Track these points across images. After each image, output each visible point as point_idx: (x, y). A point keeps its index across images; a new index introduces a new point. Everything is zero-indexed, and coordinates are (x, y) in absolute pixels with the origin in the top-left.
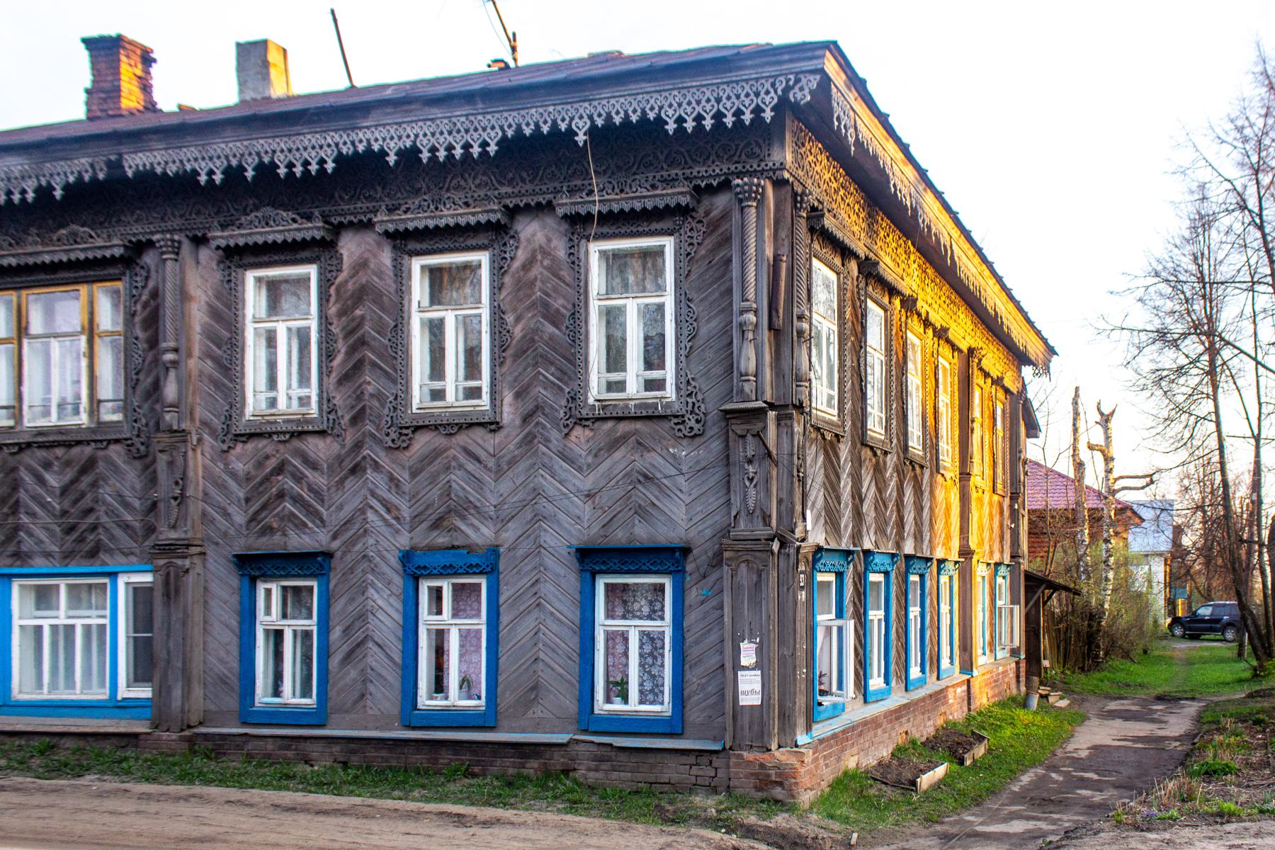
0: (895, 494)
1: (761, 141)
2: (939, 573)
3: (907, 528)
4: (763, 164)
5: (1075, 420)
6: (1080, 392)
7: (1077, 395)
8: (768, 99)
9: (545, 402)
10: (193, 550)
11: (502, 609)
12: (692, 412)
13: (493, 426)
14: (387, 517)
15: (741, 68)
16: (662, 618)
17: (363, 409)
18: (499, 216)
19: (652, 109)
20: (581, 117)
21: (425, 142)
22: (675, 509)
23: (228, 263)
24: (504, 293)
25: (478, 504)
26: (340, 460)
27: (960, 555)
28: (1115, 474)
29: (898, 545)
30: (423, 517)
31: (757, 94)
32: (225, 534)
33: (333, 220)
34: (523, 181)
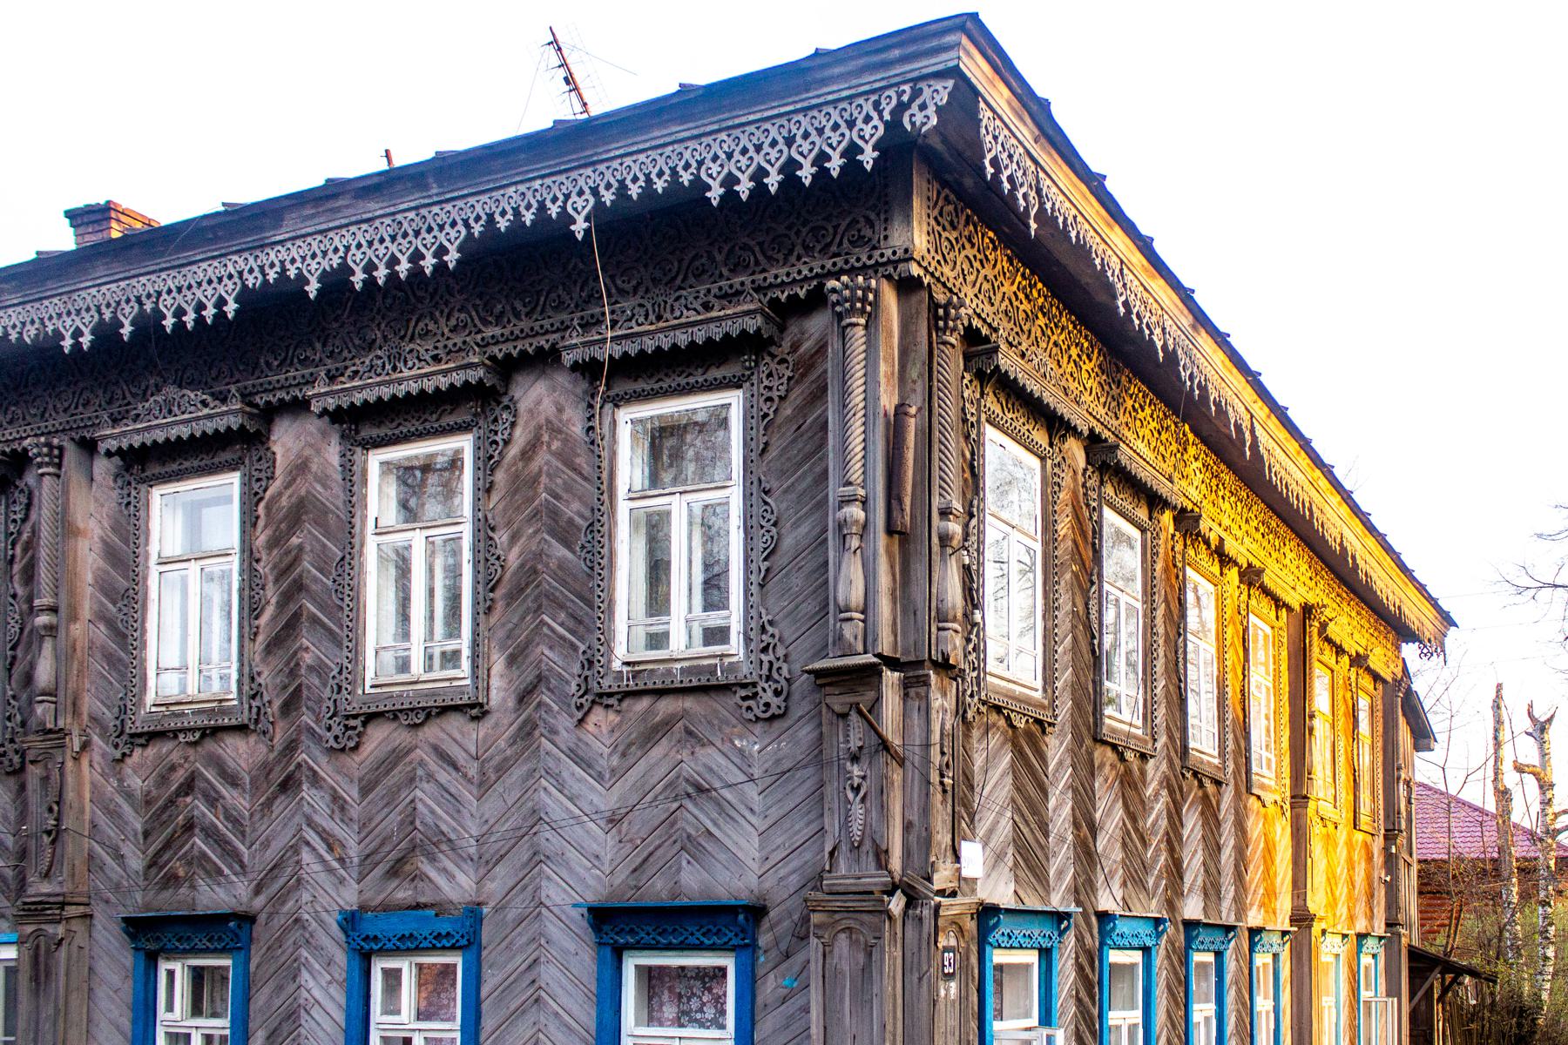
0: (1164, 823)
1: (873, 216)
2: (1251, 950)
3: (1188, 879)
4: (876, 253)
5: (1496, 730)
6: (1504, 693)
7: (1499, 695)
8: (868, 130)
9: (551, 670)
10: (71, 911)
11: (485, 1006)
12: (769, 678)
13: (476, 710)
14: (328, 857)
15: (824, 82)
16: (723, 1027)
17: (298, 689)
18: (481, 372)
19: (687, 166)
20: (581, 193)
21: (359, 256)
22: (742, 842)
23: (127, 477)
24: (495, 497)
25: (453, 837)
26: (266, 769)
27: (1292, 921)
28: (1556, 808)
29: (1171, 906)
30: (378, 857)
31: (851, 124)
32: (118, 886)
33: (257, 399)
34: (517, 316)
